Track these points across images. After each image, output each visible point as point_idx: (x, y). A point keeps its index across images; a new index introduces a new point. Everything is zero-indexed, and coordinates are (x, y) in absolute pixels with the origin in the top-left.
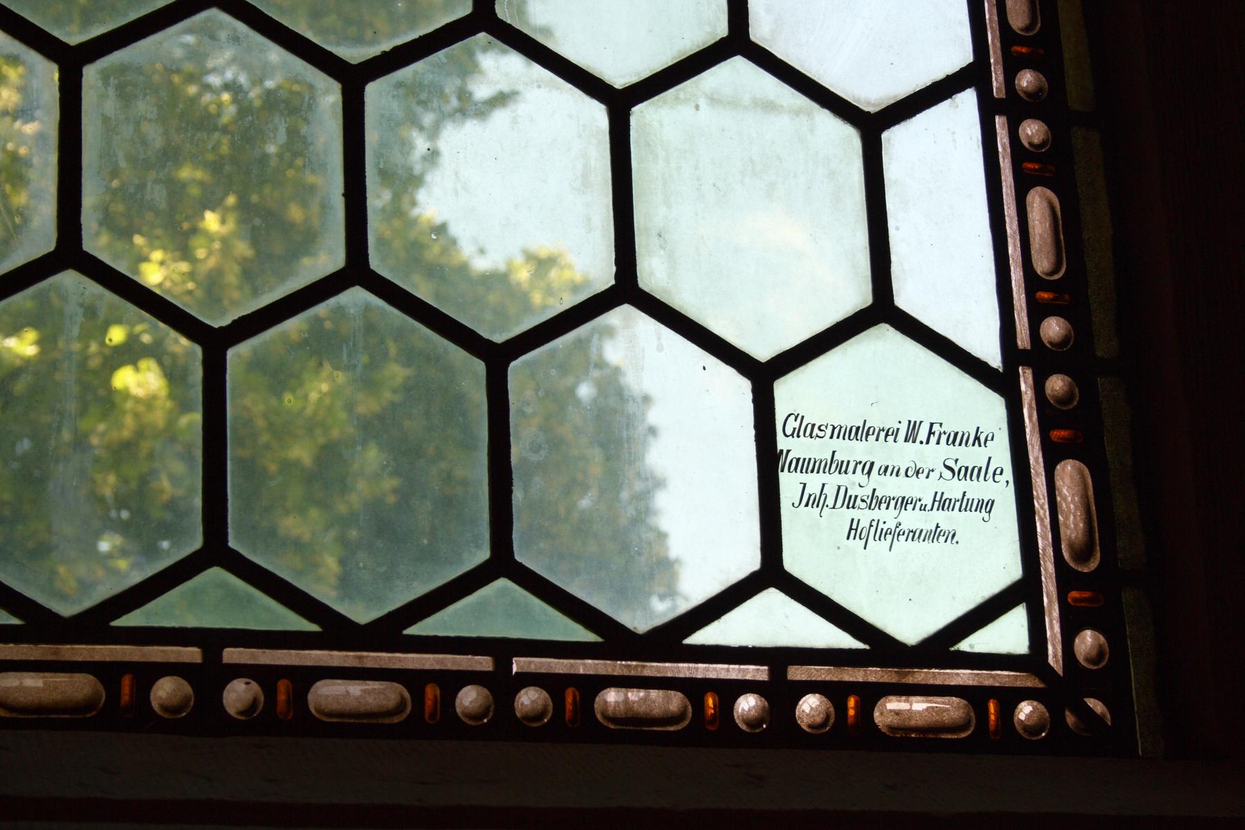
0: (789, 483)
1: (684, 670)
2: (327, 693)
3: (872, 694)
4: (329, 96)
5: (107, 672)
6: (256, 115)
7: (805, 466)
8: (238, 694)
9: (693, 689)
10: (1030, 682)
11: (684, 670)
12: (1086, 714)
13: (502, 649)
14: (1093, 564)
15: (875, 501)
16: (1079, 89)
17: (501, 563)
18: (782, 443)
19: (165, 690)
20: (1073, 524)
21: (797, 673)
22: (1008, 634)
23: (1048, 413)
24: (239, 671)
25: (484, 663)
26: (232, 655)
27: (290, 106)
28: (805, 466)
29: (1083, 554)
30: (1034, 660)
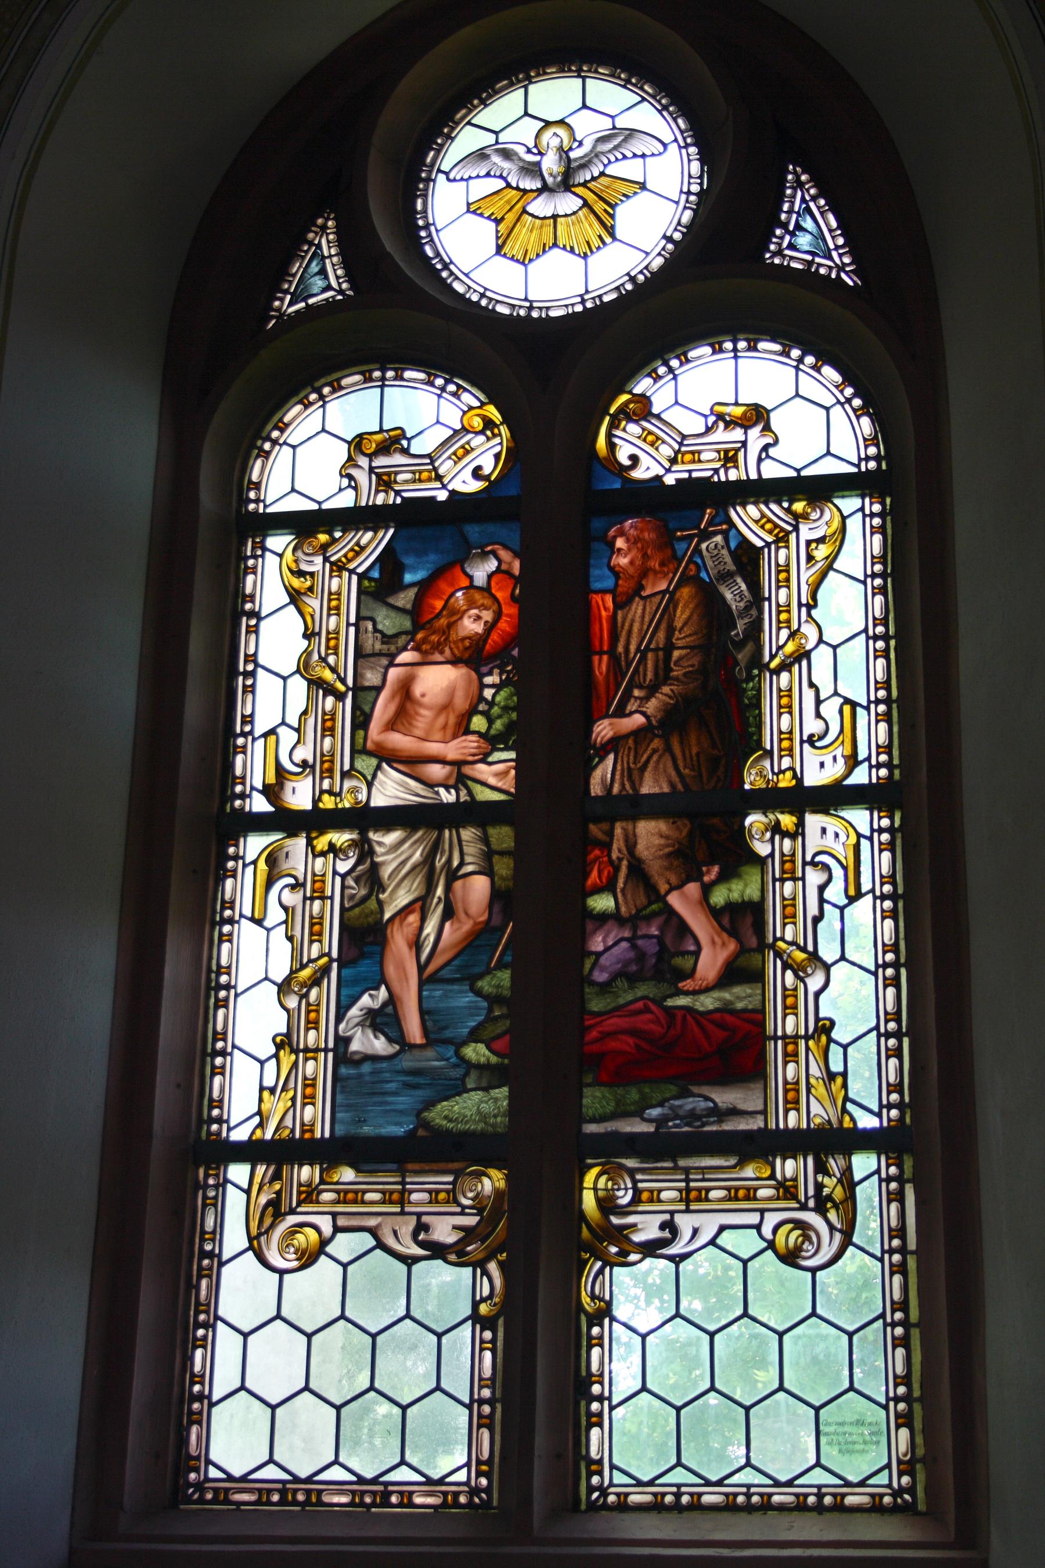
0: (823, 1440)
1: (444, 1488)
2: (776, 1499)
3: (844, 1496)
4: (706, 1338)
5: (655, 1495)
6: (689, 1344)
7: (827, 1434)
8: (685, 1499)
9: (797, 1495)
10: (889, 1491)
11: (444, 1488)
12: (480, 1499)
13: (749, 1486)
14: (908, 1457)
15: (847, 1443)
16: (914, 1315)
17: (679, 1463)
18: (821, 1428)
19: (669, 1499)
20: (903, 1448)
21: (824, 1490)
22: (461, 1476)
23: (898, 1416)
24: (393, 1492)
25: (744, 1490)
26: (683, 1489)
27: (763, 1342)
28: (827, 1434)
29: (905, 1455)
30: (467, 1483)
